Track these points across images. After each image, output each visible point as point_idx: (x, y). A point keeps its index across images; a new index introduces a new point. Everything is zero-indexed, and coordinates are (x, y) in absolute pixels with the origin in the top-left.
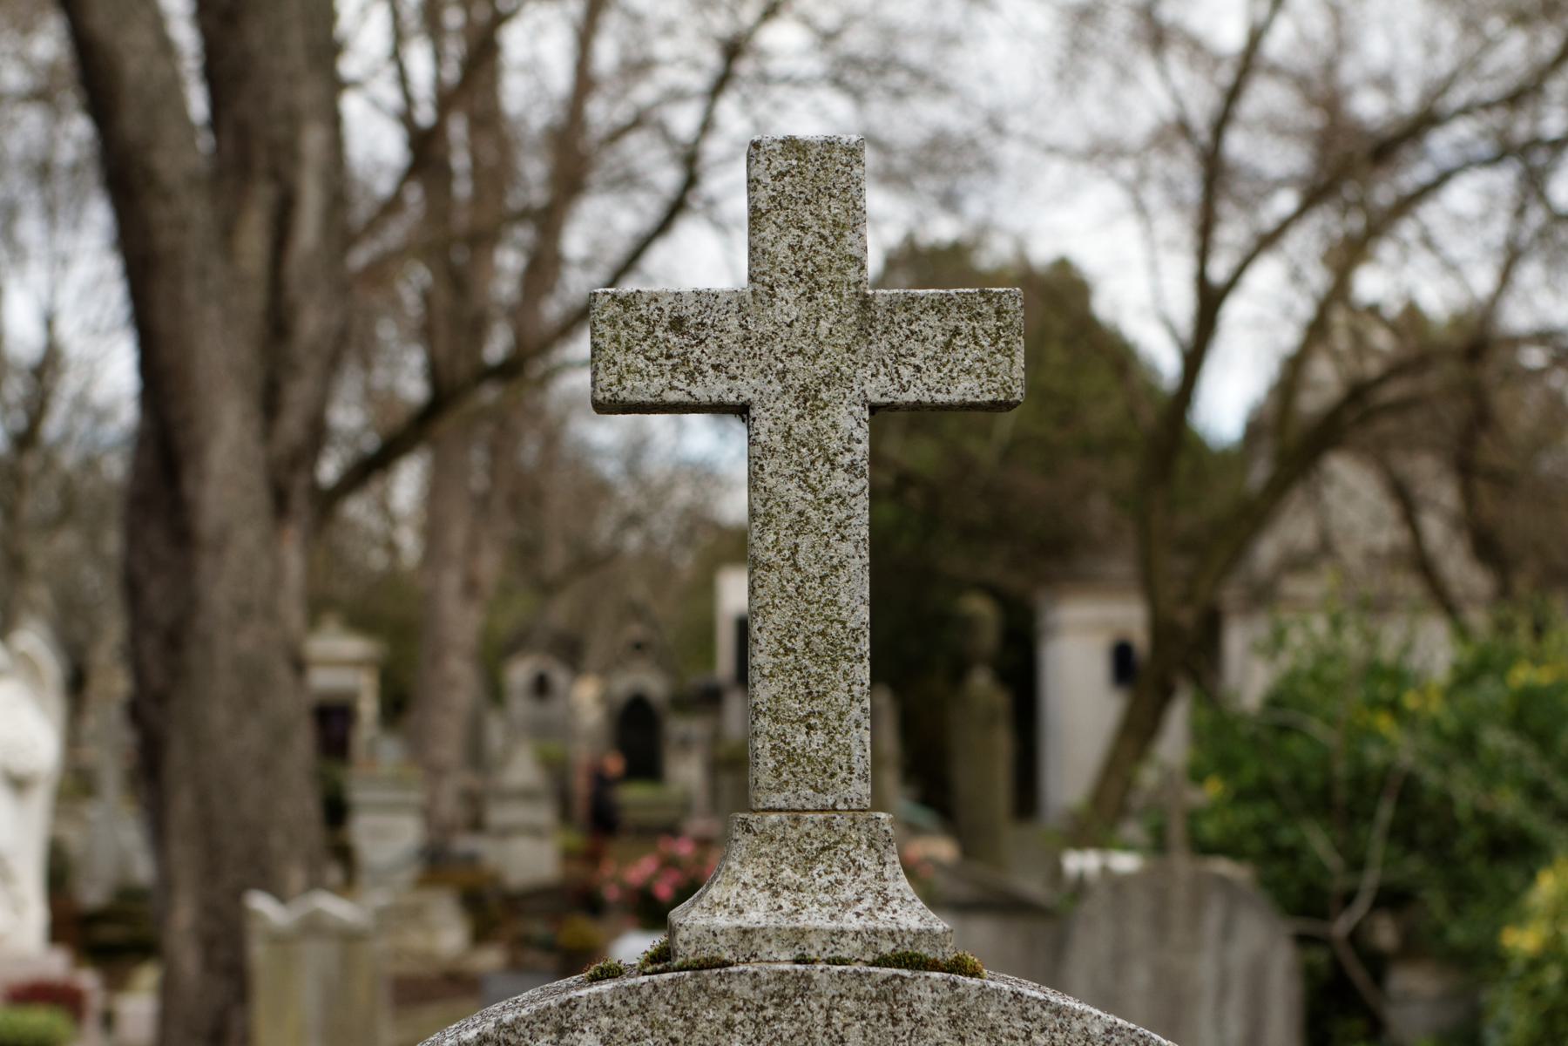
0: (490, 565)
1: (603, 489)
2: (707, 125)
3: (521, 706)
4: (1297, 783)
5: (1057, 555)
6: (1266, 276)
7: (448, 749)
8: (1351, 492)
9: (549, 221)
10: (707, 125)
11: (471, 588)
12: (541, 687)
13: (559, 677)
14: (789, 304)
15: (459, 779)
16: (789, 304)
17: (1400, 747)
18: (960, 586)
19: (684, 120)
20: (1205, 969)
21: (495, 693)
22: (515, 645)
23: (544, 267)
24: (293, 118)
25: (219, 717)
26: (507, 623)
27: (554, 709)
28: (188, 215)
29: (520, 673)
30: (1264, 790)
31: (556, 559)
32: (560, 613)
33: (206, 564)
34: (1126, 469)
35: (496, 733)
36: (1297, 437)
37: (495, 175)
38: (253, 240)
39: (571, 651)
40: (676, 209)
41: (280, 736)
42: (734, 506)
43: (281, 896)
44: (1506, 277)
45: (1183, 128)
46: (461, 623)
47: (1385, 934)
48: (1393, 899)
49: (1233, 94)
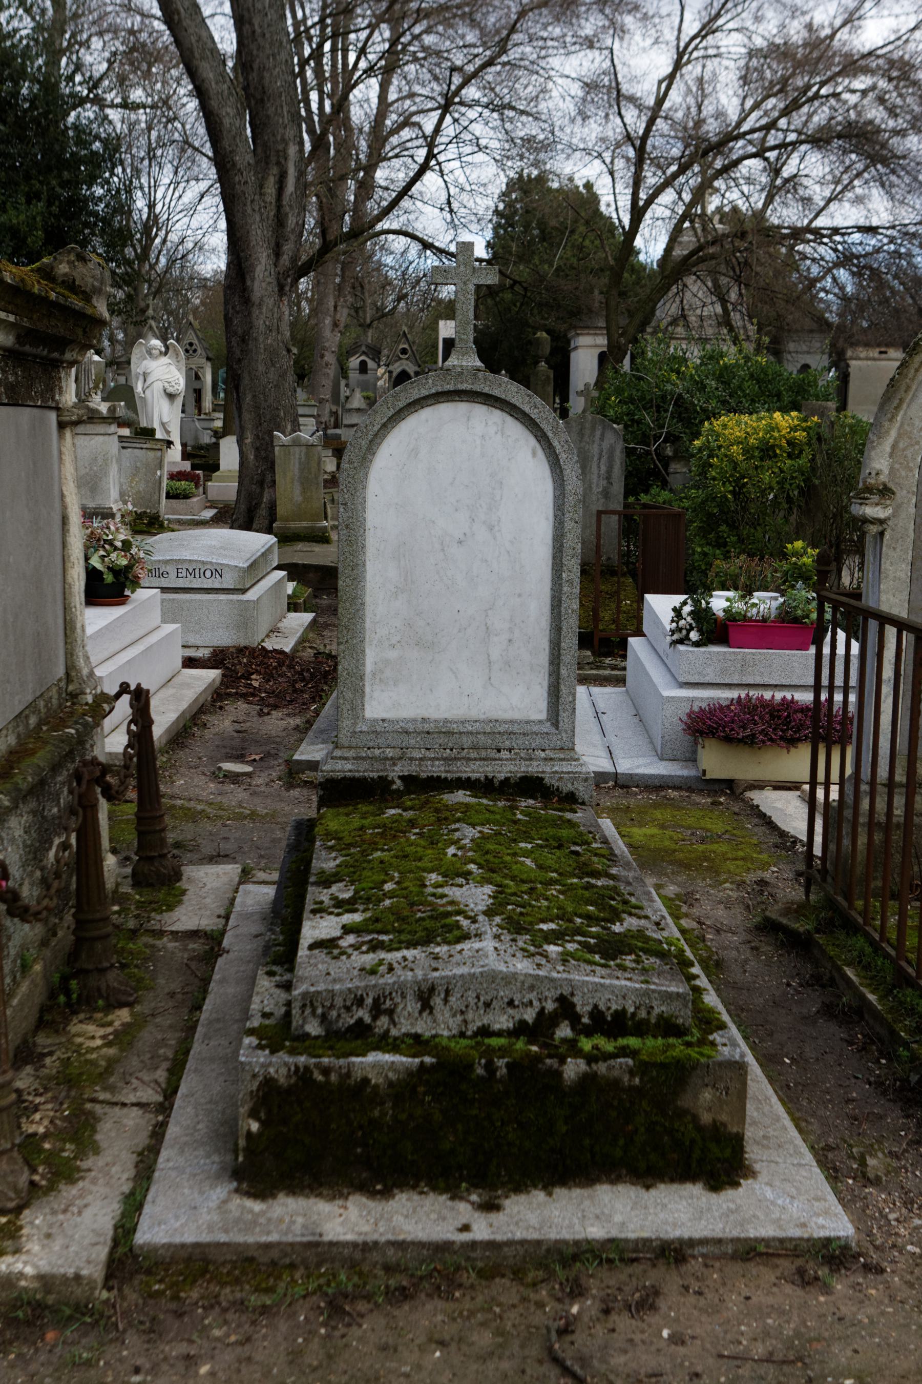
0: (343, 315)
1: (388, 282)
2: (437, 130)
3: (354, 376)
4: (642, 398)
5: (577, 317)
6: (668, 197)
7: (326, 394)
8: (696, 292)
9: (370, 169)
10: (437, 130)
11: (335, 325)
12: (363, 368)
13: (371, 364)
14: (462, 268)
15: (328, 407)
16: (462, 268)
17: (678, 386)
18: (536, 329)
19: (429, 125)
20: (595, 449)
21: (343, 371)
22: (350, 353)
23: (366, 187)
24: (285, 141)
25: (261, 368)
26: (348, 341)
27: (369, 376)
28: (247, 179)
29: (354, 362)
30: (631, 400)
31: (369, 314)
32: (370, 336)
33: (255, 312)
34: (605, 280)
35: (344, 391)
36: (673, 269)
37: (346, 146)
38: (270, 189)
39: (375, 353)
40: (424, 168)
41: (283, 376)
42: (832, 318)
43: (283, 433)
44: (769, 200)
45: (628, 137)
46: (331, 340)
47: (669, 451)
48: (672, 438)
49: (651, 122)
